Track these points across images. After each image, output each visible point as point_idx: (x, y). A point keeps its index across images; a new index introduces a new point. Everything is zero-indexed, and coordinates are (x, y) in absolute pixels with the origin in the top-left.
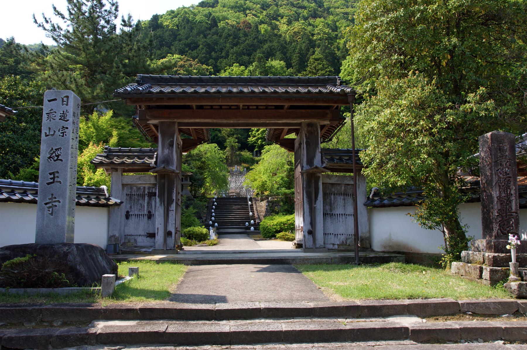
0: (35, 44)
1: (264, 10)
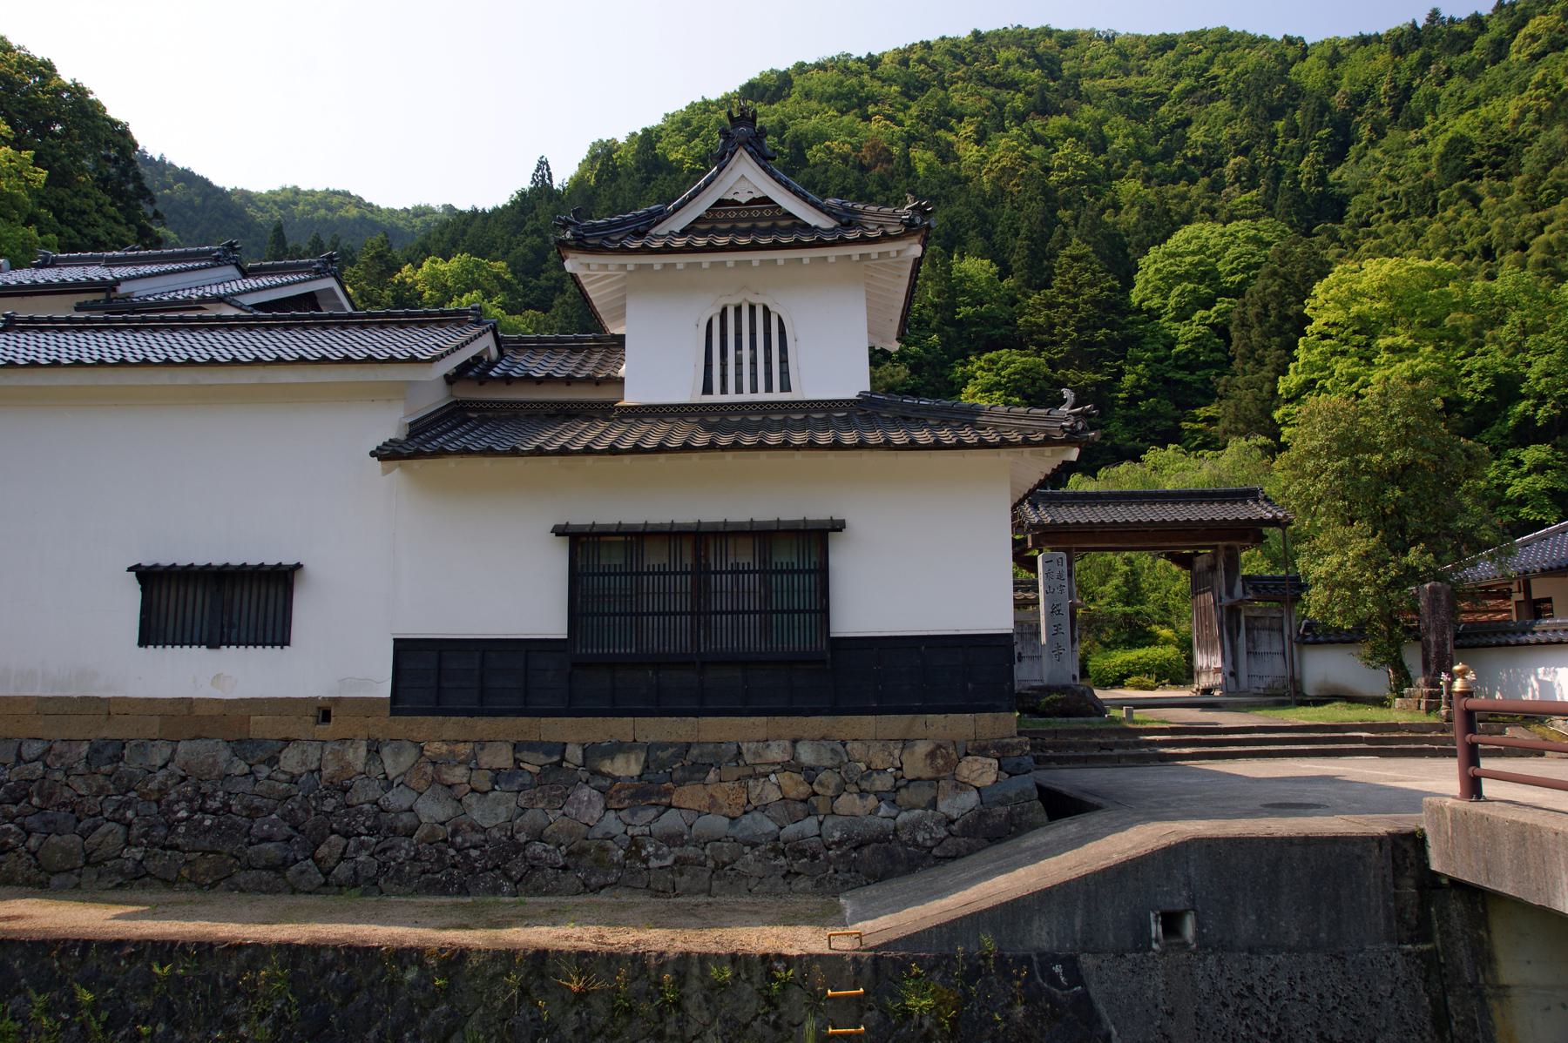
0: (284, 189)
1: (913, 99)
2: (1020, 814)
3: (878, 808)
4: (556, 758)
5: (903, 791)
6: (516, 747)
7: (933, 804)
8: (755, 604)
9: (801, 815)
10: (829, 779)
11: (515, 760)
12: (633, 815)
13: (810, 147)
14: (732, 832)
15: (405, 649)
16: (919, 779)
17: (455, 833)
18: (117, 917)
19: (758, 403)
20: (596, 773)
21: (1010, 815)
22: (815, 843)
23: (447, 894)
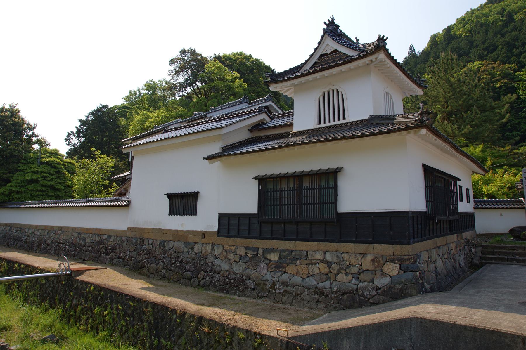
2: (406, 289)
3: (352, 280)
4: (255, 253)
5: (362, 274)
6: (246, 248)
7: (372, 281)
8: (316, 201)
9: (324, 280)
10: (335, 267)
11: (246, 253)
12: (274, 274)
13: (516, 14)
14: (302, 283)
15: (221, 216)
16: (368, 270)
17: (229, 274)
18: (142, 288)
19: (340, 124)
20: (266, 258)
21: (402, 290)
22: (328, 291)
23: (223, 293)
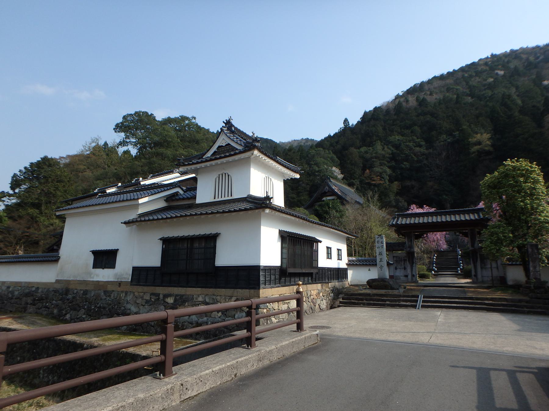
15: (135, 269)
